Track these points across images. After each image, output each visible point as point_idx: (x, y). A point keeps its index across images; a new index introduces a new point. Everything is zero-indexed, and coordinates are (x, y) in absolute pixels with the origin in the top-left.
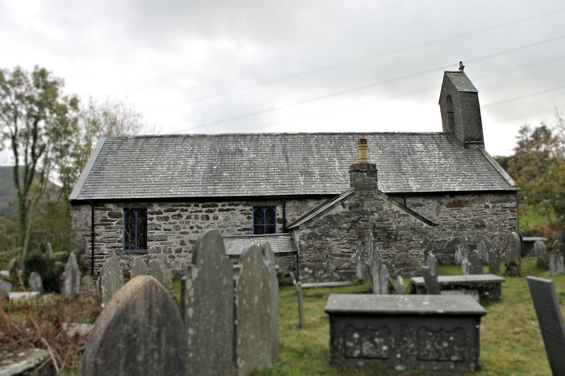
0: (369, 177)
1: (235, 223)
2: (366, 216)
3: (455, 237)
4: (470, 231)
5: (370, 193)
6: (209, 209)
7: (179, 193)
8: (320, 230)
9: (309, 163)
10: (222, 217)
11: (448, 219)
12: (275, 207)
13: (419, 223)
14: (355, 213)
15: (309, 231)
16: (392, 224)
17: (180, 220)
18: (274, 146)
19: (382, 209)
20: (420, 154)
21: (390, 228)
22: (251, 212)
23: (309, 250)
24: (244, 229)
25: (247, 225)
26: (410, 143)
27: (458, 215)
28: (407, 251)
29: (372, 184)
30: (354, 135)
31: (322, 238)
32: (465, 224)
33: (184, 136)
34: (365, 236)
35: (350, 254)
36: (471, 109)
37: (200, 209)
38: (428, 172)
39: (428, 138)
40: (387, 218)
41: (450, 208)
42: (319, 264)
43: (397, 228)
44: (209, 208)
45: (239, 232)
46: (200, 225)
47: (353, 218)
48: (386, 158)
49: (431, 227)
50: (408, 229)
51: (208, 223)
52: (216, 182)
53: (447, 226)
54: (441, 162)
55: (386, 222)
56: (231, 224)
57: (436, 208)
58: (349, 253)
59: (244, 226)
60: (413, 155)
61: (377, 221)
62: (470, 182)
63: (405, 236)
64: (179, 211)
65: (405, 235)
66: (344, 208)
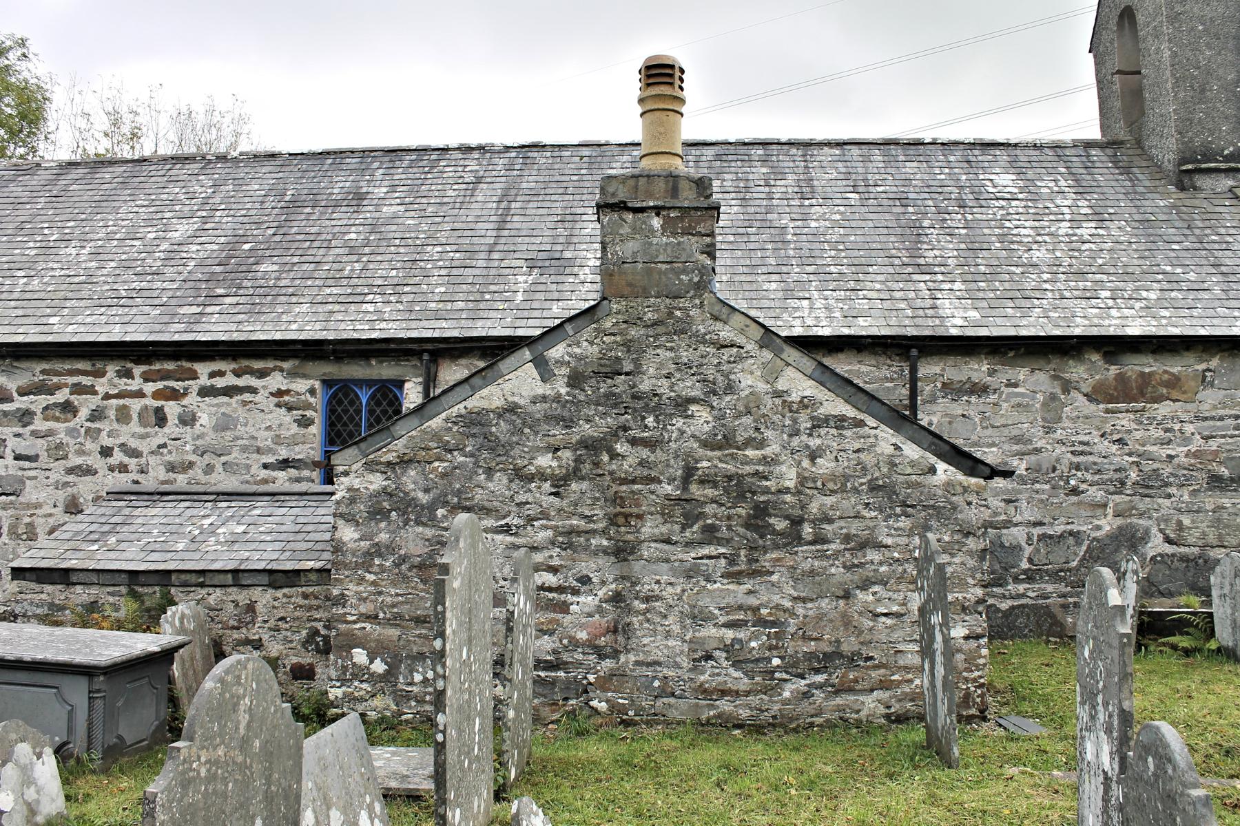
0: (674, 234)
1: (253, 438)
2: (650, 421)
3: (1119, 521)
4: (1186, 498)
5: (678, 313)
6: (166, 387)
7: (70, 329)
8: (426, 479)
9: (577, 232)
10: (210, 415)
11: (1095, 449)
12: (400, 384)
13: (912, 464)
14: (598, 404)
15: (376, 482)
16: (773, 461)
17: (71, 424)
18: (479, 181)
19: (730, 388)
20: (1002, 207)
21: (766, 479)
22: (312, 400)
23: (375, 569)
24: (285, 464)
25: (297, 448)
26: (971, 171)
27: (1138, 435)
28: (847, 596)
29: (684, 271)
30: (774, 147)
31: (433, 518)
32: (1167, 470)
33: (209, 157)
34: (640, 517)
35: (563, 597)
36: (1207, 45)
37: (135, 384)
38: (1023, 265)
39: (1041, 159)
40: (751, 433)
41: (1101, 406)
42: (419, 636)
43: (802, 480)
44: (166, 383)
45: (267, 472)
46: (133, 443)
47: (585, 429)
48: (871, 216)
49: (973, 480)
50: (856, 490)
51: (161, 436)
52: (220, 291)
53: (1089, 477)
54: (1078, 231)
55: (751, 453)
56: (240, 442)
57: (1044, 404)
58: (560, 589)
59: (284, 453)
60: (975, 210)
61: (705, 444)
62: (1192, 304)
63: (842, 523)
64: (67, 391)
65: (841, 518)
66: (544, 380)
